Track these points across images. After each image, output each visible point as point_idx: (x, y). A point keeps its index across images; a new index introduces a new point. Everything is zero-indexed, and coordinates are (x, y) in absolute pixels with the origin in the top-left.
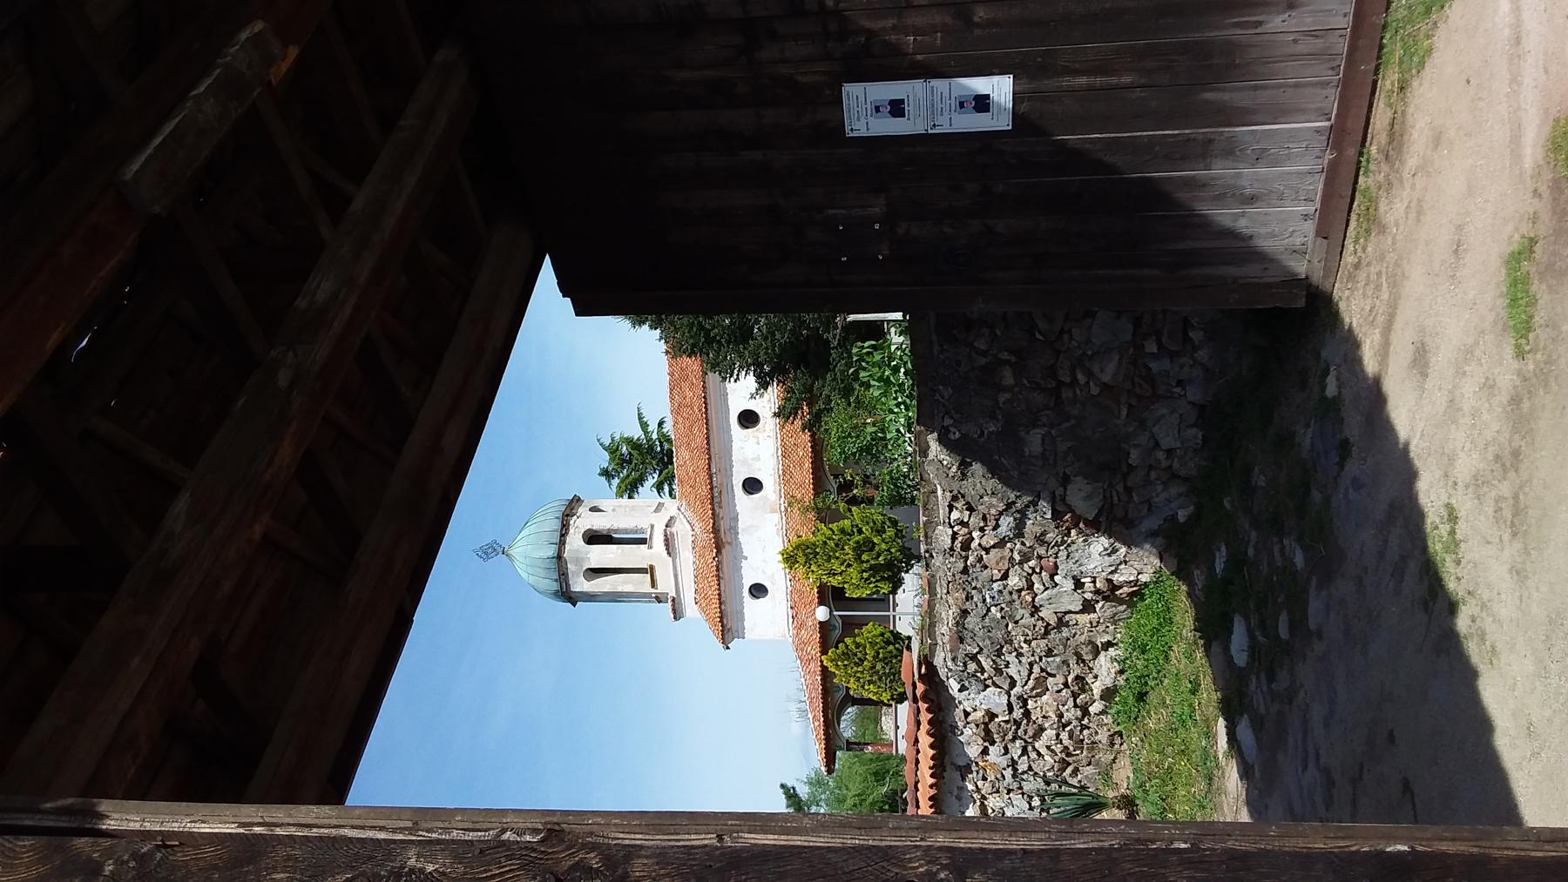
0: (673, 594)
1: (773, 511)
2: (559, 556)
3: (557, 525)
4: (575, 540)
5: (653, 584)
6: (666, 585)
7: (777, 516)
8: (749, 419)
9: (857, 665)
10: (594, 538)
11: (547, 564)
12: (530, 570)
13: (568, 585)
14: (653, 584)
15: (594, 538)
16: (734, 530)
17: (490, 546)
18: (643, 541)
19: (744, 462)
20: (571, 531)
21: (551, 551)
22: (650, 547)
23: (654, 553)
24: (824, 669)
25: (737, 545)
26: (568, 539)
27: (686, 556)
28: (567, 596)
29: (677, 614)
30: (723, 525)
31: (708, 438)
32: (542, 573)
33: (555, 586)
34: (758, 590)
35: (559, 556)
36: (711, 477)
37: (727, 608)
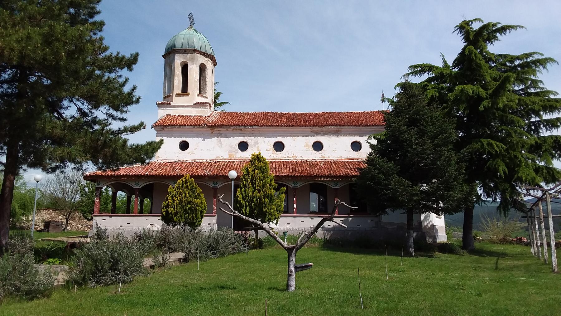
0: (172, 104)
1: (230, 156)
2: (194, 50)
3: (209, 52)
4: (202, 59)
5: (178, 95)
6: (177, 101)
7: (227, 157)
8: (356, 146)
9: (271, 201)
10: (202, 68)
11: (191, 44)
12: (186, 36)
13: (179, 53)
14: (178, 95)
15: (202, 68)
16: (220, 135)
17: (193, 21)
18: (200, 92)
19: (257, 143)
20: (206, 59)
21: (197, 47)
22: (198, 95)
23: (194, 96)
24: (181, 177)
25: (212, 136)
26: (202, 56)
27: (194, 113)
28: (170, 53)
29: (160, 105)
30: (223, 130)
31: (378, 125)
32: (186, 41)
33: (178, 46)
34: (184, 146)
35: (194, 50)
36: (250, 126)
37: (176, 129)
